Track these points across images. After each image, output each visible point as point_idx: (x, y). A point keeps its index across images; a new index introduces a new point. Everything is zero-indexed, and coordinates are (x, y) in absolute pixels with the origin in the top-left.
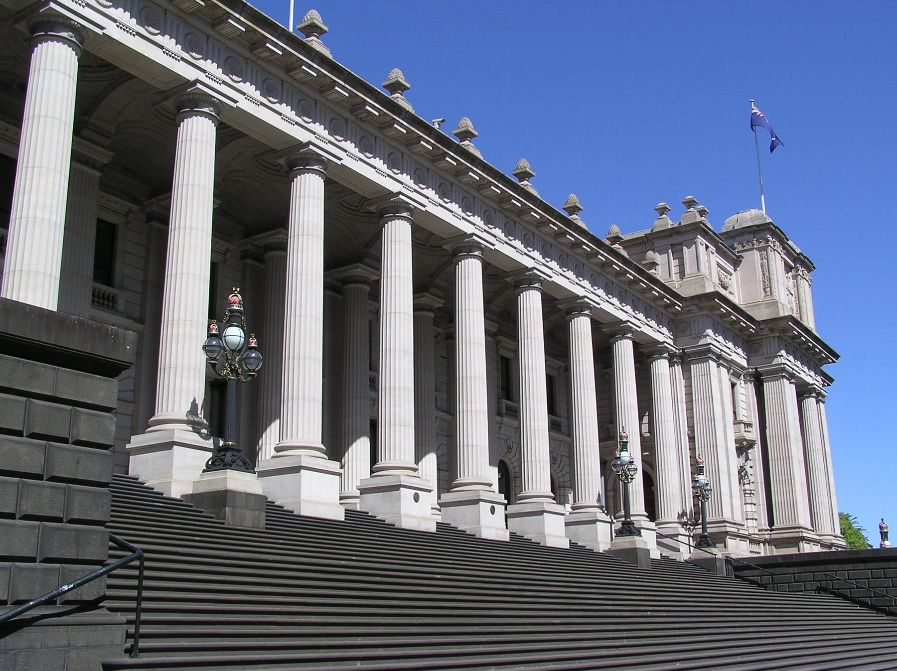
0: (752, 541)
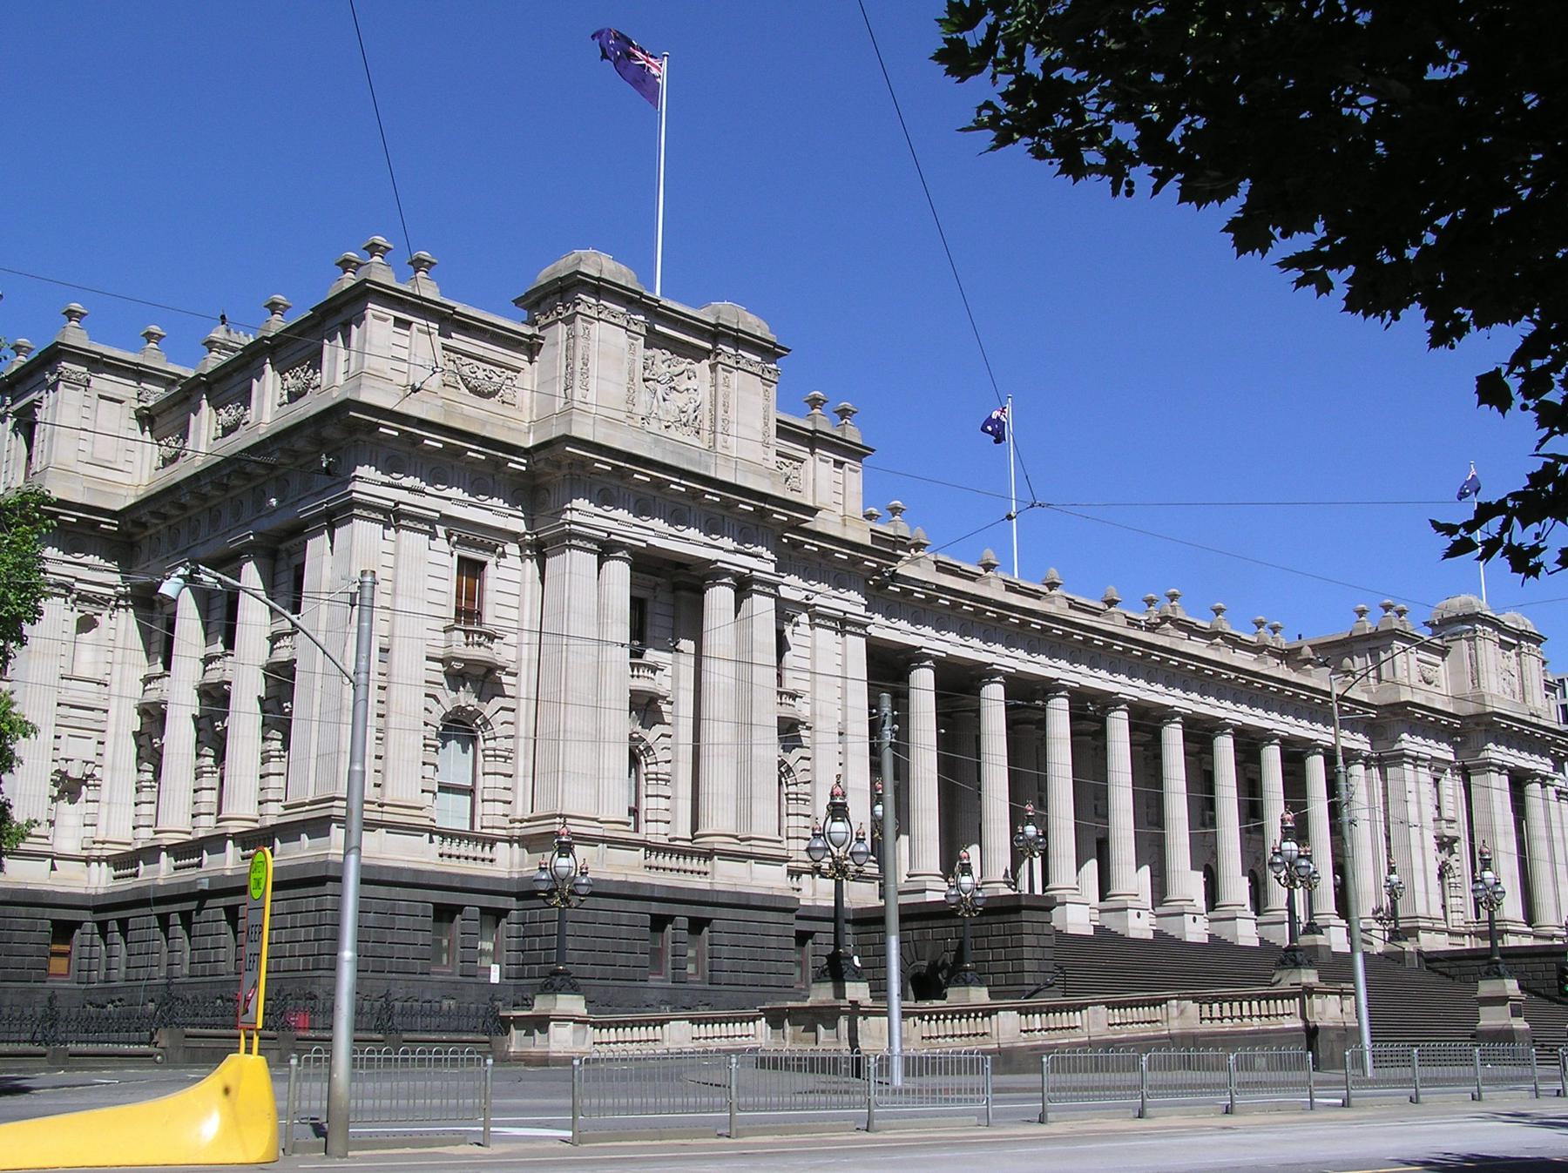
0: (1451, 934)
